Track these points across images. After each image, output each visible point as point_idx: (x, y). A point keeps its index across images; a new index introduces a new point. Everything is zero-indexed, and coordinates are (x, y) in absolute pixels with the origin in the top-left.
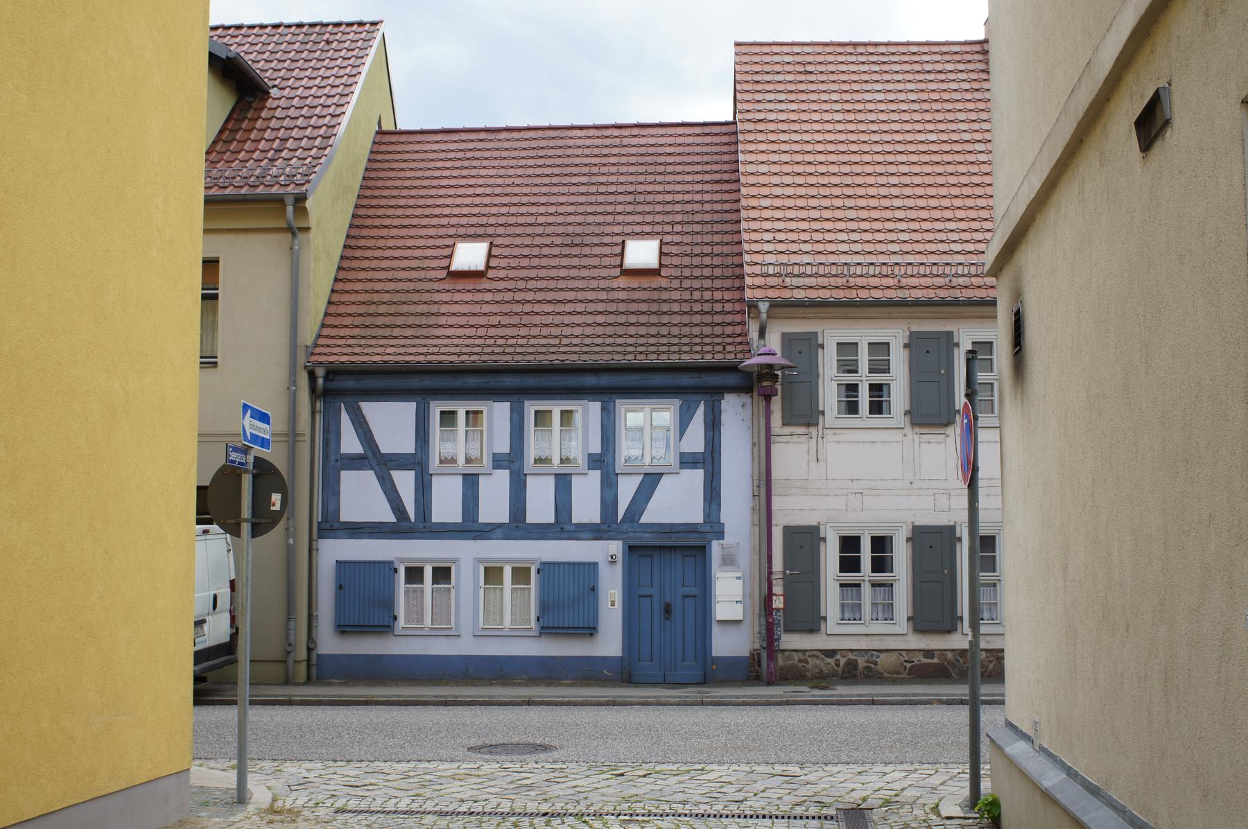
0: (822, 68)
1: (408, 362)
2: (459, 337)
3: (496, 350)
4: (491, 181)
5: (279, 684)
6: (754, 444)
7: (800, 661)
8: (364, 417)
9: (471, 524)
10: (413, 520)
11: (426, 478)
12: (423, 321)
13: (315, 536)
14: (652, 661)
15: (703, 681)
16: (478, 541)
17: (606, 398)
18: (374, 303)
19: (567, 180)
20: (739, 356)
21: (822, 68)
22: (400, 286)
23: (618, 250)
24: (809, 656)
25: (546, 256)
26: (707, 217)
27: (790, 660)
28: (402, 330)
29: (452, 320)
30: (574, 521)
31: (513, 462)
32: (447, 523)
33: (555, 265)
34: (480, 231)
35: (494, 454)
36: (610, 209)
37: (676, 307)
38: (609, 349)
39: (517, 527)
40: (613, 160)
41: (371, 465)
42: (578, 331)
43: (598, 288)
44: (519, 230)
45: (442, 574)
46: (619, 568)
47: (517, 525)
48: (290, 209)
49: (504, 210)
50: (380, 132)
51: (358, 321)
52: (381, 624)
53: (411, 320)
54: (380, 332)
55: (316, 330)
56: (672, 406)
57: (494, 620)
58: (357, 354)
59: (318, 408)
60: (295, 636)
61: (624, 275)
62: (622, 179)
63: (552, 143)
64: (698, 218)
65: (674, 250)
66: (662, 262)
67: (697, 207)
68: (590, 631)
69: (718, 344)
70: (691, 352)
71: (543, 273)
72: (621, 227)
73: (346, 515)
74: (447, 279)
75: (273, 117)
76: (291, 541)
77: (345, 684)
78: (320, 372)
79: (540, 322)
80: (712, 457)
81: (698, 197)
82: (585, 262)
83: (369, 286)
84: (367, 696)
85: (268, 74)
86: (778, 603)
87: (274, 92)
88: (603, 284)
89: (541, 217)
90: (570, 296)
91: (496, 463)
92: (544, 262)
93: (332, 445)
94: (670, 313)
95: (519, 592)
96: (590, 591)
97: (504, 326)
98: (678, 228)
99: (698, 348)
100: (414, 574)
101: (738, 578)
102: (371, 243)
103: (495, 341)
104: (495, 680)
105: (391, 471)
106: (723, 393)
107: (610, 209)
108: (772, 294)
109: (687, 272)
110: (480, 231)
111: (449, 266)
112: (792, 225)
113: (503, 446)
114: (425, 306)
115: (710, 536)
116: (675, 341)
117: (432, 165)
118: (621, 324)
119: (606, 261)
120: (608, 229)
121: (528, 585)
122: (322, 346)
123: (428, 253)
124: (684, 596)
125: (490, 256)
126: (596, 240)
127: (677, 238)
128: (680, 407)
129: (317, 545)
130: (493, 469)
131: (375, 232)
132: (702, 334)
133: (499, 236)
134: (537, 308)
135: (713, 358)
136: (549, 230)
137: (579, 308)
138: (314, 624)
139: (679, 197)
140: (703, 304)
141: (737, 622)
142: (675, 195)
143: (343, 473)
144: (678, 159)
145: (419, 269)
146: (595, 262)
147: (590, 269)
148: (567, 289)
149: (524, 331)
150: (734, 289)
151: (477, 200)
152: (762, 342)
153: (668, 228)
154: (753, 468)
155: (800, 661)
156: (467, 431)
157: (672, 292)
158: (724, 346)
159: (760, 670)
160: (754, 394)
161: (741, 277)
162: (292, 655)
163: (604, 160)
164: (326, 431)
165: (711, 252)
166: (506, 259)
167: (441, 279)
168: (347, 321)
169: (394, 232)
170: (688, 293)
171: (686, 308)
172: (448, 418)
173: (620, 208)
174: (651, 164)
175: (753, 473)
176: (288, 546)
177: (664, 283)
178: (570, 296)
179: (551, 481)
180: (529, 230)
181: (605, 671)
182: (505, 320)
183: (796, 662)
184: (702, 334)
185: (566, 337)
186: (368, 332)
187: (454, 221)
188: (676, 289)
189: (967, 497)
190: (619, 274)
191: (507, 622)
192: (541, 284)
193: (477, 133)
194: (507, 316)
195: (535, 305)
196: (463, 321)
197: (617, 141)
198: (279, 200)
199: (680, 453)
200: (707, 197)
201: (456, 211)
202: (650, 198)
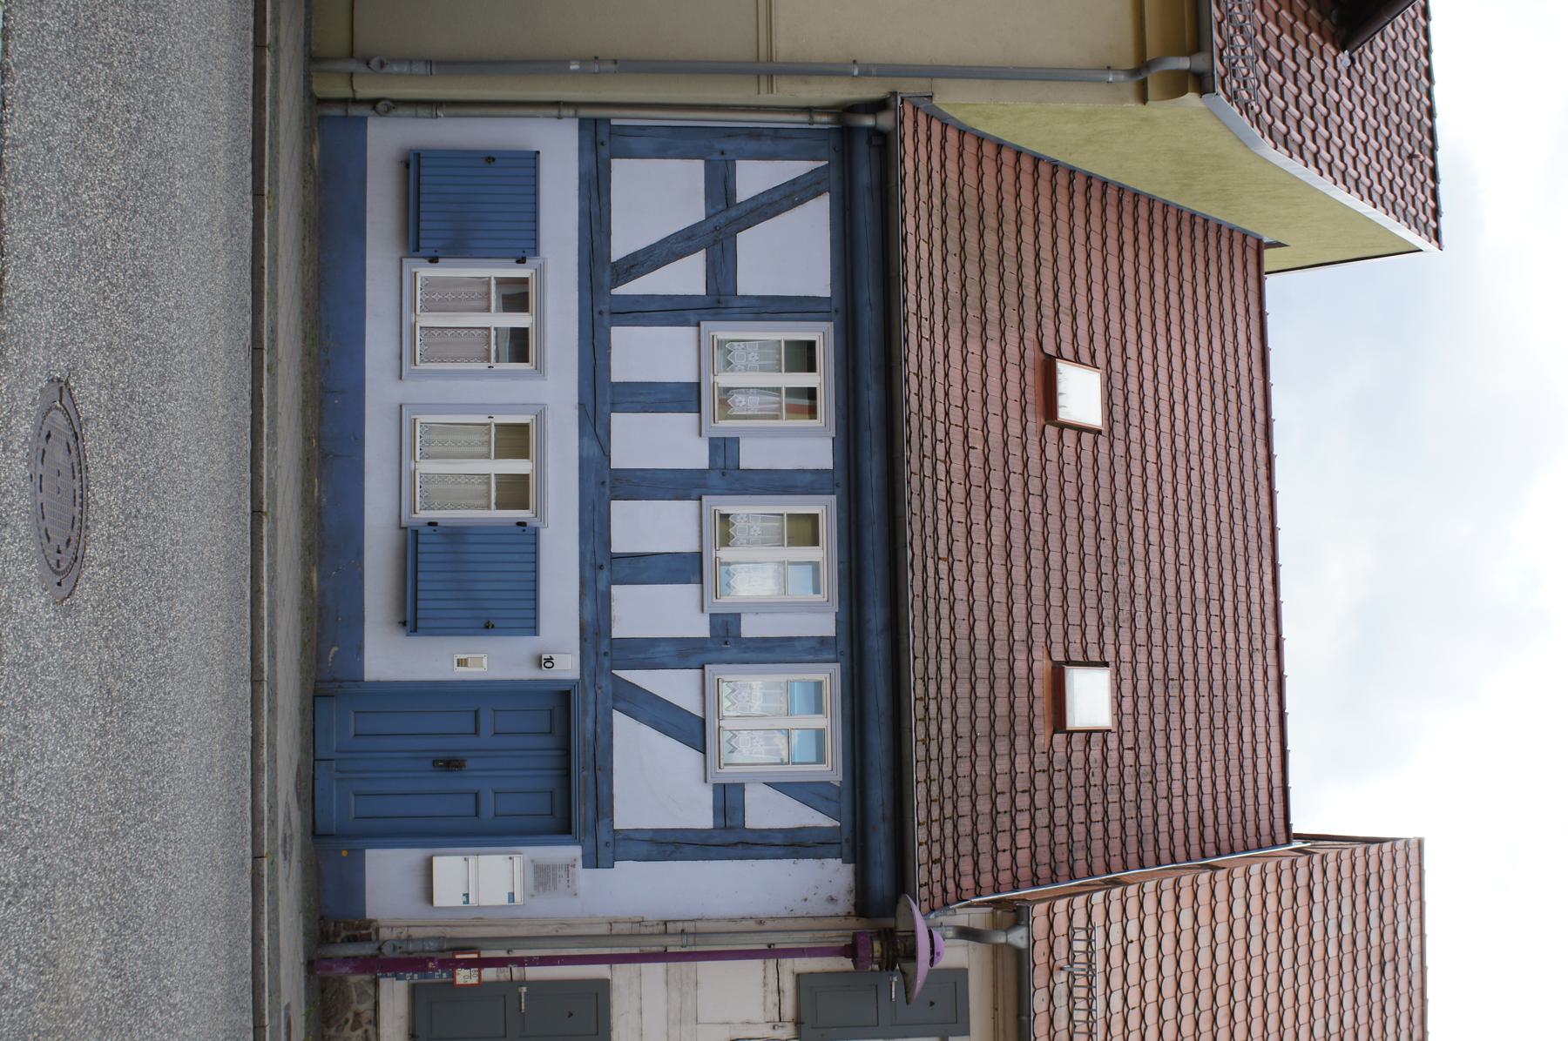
0: (1389, 991)
1: (905, 280)
2: (946, 375)
3: (927, 443)
4: (1194, 432)
5: (308, 43)
6: (761, 922)
7: (357, 1015)
8: (802, 202)
9: (608, 398)
10: (615, 292)
11: (692, 316)
12: (973, 312)
13: (584, 113)
14: (356, 735)
15: (317, 832)
16: (576, 412)
17: (843, 645)
18: (1000, 225)
19: (1199, 561)
20: (924, 890)
21: (1389, 991)
22: (1029, 272)
23: (1094, 655)
24: (366, 1031)
25: (1081, 527)
26: (1147, 808)
27: (358, 996)
28: (958, 274)
29: (974, 363)
30: (615, 589)
31: (723, 474)
32: (610, 353)
33: (1068, 546)
34: (1118, 414)
35: (737, 440)
36: (1157, 638)
37: (1002, 765)
38: (932, 650)
39: (603, 483)
40: (1230, 637)
41: (715, 215)
42: (961, 590)
43: (1032, 623)
44: (1120, 480)
45: (519, 345)
46: (528, 673)
47: (607, 483)
48: (1184, 63)
49: (1151, 454)
50: (1260, 246)
51: (971, 194)
52: (421, 233)
53: (973, 290)
54: (953, 234)
55: (959, 115)
56: (829, 768)
57: (429, 443)
58: (917, 188)
59: (818, 118)
60: (399, 74)
61: (1053, 668)
62: (1202, 655)
63: (1252, 532)
64: (1146, 791)
65: (1096, 754)
66: (1075, 735)
67: (1162, 788)
68: (411, 621)
69: (943, 849)
70: (929, 801)
71: (1054, 524)
72: (1128, 659)
73: (622, 169)
74: (1041, 355)
75: (1312, 54)
76: (574, 67)
77: (307, 165)
78: (885, 121)
79: (974, 521)
80: (736, 844)
81: (1177, 788)
82: (1073, 598)
83: (1028, 218)
84: (275, 198)
85: (1367, 51)
86: (464, 977)
87: (1344, 59)
88: (1038, 631)
89: (1142, 517)
90: (1019, 574)
91: (721, 443)
92: (1072, 526)
93: (752, 145)
94: (993, 754)
95: (484, 487)
96: (486, 621)
97: (967, 456)
98: (1129, 758)
99: (935, 813)
100: (516, 297)
101: (511, 896)
102: (1096, 224)
103: (941, 441)
104: (319, 446)
105: (704, 250)
106: (854, 862)
107: (1157, 638)
108: (1041, 949)
109: (1059, 780)
110: (1118, 414)
111: (1062, 358)
112: (1151, 972)
113: (753, 456)
114: (997, 315)
115: (590, 842)
116: (947, 769)
117: (1216, 331)
118: (973, 668)
119: (1074, 635)
120: (1125, 635)
121: (496, 504)
122: (929, 128)
123: (1082, 322)
124: (477, 795)
125: (1080, 429)
126: (1108, 614)
127: (1113, 758)
128: (828, 783)
129: (568, 117)
130: (711, 439)
131: (1112, 231)
132: (959, 817)
133: (1112, 446)
134: (998, 515)
135: (920, 844)
136: (1122, 532)
137: (997, 590)
138: (422, 111)
139: (1176, 756)
140: (1008, 815)
141: (429, 896)
142: (1179, 749)
143: (699, 165)
144: (1233, 749)
145: (1056, 305)
146: (1074, 617)
147: (1062, 606)
148: (1028, 567)
149: (958, 492)
150: (1034, 866)
151: (1164, 407)
152: (950, 933)
153: (1128, 741)
154: (718, 920)
155: (357, 1015)
156: (778, 390)
157: (1027, 756)
158: (939, 861)
159: (339, 940)
160: (854, 919)
161: (1054, 877)
162: (363, 68)
163: (1229, 622)
164: (776, 134)
165: (1093, 819)
166: (1075, 459)
167: (1041, 344)
168: (970, 176)
169: (1113, 263)
170: (1026, 785)
171: (1002, 783)
172: (803, 357)
173: (1157, 654)
174: (1225, 704)
175: (708, 920)
176: (567, 62)
177: (1041, 741)
178: (1019, 574)
179: (688, 545)
180: (1121, 497)
181: (335, 649)
182: (976, 458)
183: (355, 1007)
184: (959, 817)
185: (951, 569)
186: (953, 213)
187: (1132, 367)
188: (1032, 763)
189: (643, 965)
190: (1055, 659)
191: (425, 467)
192: (1036, 520)
193: (1263, 408)
194: (983, 461)
195: (1002, 512)
196: (974, 382)
197: (1257, 644)
198: (1198, 43)
199: (743, 784)
200: (1178, 804)
201: (1148, 372)
202: (1174, 706)
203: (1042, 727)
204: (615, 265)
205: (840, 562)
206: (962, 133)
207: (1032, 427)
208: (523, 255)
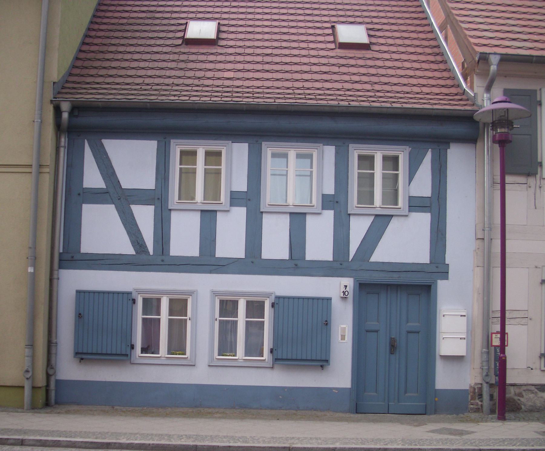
59: (63, 144)
78: (65, 107)
124: (409, 332)
125: (219, 31)
128: (410, 154)
129: (58, 274)
138: (53, 351)
155: (515, 394)
164: (69, 166)
203: (368, 54)
204: (137, 252)
205: (297, 142)
206: (71, 75)
207: (220, 50)
208: (131, 300)
